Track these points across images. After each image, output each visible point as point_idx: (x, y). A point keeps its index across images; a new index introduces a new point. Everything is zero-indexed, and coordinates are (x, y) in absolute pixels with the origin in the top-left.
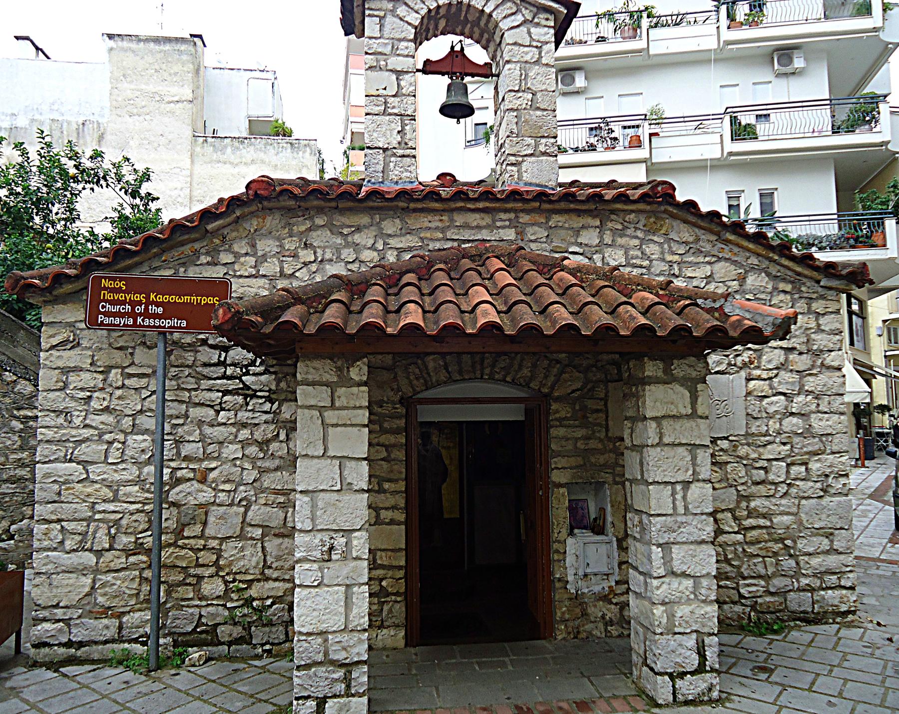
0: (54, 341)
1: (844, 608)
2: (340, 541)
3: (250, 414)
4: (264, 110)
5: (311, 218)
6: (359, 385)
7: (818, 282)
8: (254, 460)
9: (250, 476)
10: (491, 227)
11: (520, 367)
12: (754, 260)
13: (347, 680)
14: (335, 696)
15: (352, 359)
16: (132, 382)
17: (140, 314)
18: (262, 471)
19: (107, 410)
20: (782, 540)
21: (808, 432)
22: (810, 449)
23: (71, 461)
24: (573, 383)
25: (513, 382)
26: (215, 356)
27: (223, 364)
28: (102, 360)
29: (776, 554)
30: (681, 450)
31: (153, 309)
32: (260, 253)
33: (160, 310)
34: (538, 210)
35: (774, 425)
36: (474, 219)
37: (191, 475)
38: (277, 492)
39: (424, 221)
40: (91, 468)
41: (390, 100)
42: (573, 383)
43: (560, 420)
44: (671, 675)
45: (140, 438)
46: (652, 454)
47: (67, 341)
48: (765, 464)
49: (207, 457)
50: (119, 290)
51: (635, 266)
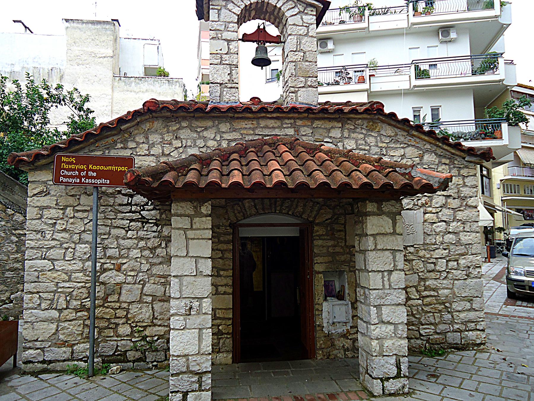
0: (35, 192)
1: (478, 342)
2: (196, 304)
3: (145, 233)
5: (179, 123)
6: (207, 216)
7: (464, 158)
8: (147, 259)
9: (145, 267)
10: (280, 128)
12: (428, 146)
14: (193, 391)
15: (202, 201)
17: (83, 177)
18: (152, 265)
19: (65, 230)
20: (444, 303)
21: (458, 243)
23: (44, 259)
24: (326, 215)
25: (293, 215)
26: (125, 200)
29: (440, 311)
30: (387, 253)
31: (90, 173)
33: (95, 174)
35: (439, 239)
37: (112, 267)
38: (160, 276)
40: (56, 263)
42: (326, 215)
44: (381, 379)
46: (371, 255)
48: (434, 261)
49: (121, 257)
50: (72, 163)
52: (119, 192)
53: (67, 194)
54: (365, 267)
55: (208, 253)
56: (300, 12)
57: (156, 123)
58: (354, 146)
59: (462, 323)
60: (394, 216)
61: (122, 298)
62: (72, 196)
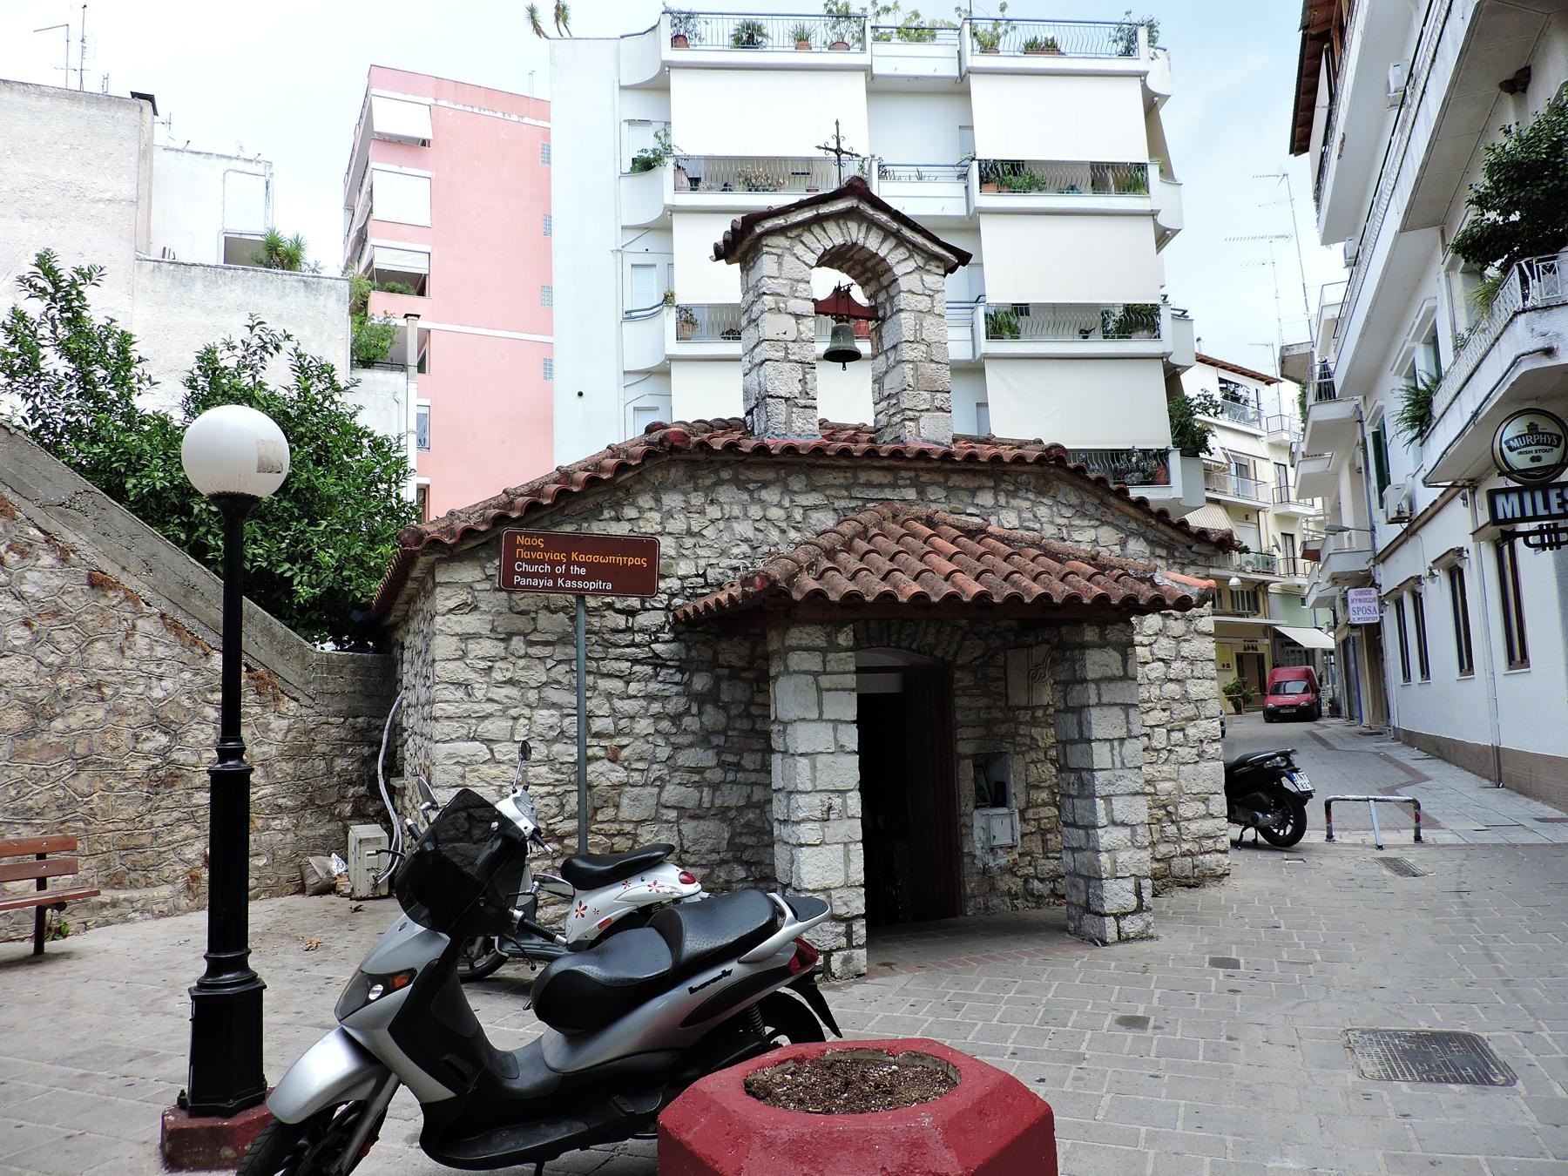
0: (452, 604)
1: (1220, 871)
2: (837, 801)
3: (660, 686)
4: (253, 226)
5: (716, 471)
6: (846, 650)
7: (1190, 547)
8: (666, 736)
9: (663, 753)
10: (894, 486)
11: (925, 633)
12: (1133, 525)
13: (849, 934)
14: (839, 949)
15: (839, 626)
16: (533, 651)
17: (561, 575)
18: (677, 748)
19: (510, 682)
20: (1165, 807)
21: (1186, 698)
22: (1187, 714)
23: (474, 739)
24: (973, 650)
25: (918, 651)
26: (621, 621)
27: (629, 630)
28: (503, 625)
29: (1159, 820)
30: (1116, 709)
31: (575, 569)
32: (665, 508)
33: (583, 571)
34: (937, 470)
35: (1155, 691)
36: (877, 477)
37: (602, 753)
38: (692, 770)
39: (829, 478)
40: (496, 747)
41: (791, 345)
42: (973, 650)
43: (965, 689)
44: (1115, 915)
45: (545, 712)
46: (1095, 714)
47: (465, 604)
48: (1148, 730)
49: (619, 733)
50: (536, 549)
51: (1028, 529)
52: (610, 606)
53: (510, 609)
54: (1081, 732)
55: (852, 714)
56: (918, 268)
57: (673, 471)
58: (1016, 523)
59: (1194, 840)
60: (1126, 648)
61: (625, 813)
62: (522, 613)
